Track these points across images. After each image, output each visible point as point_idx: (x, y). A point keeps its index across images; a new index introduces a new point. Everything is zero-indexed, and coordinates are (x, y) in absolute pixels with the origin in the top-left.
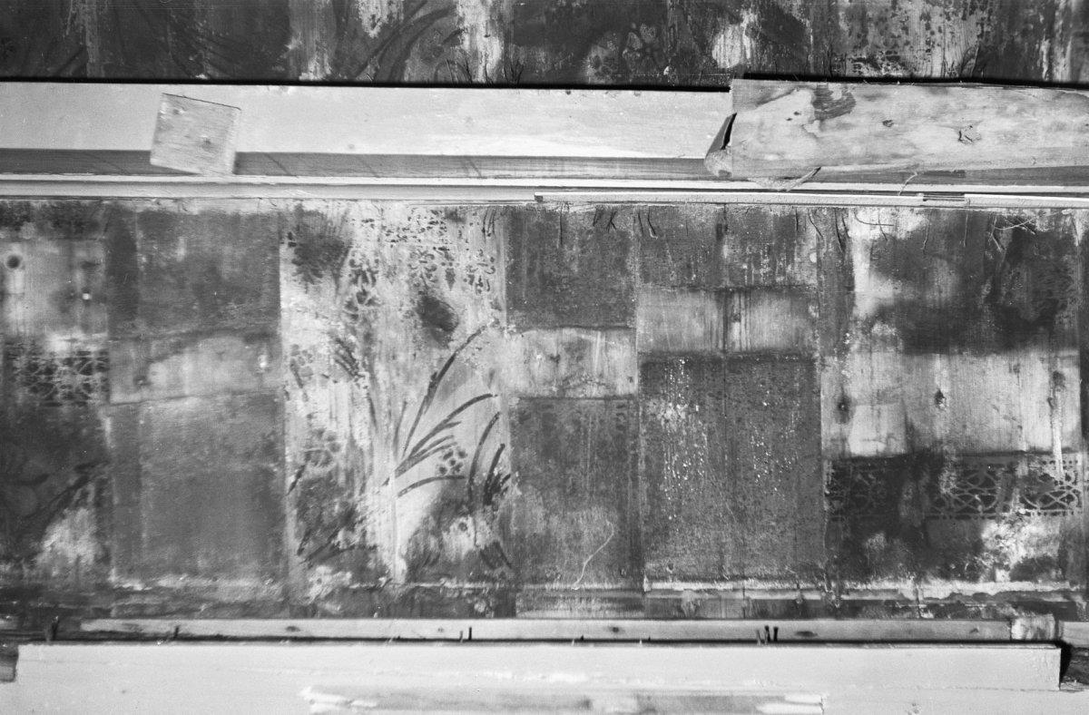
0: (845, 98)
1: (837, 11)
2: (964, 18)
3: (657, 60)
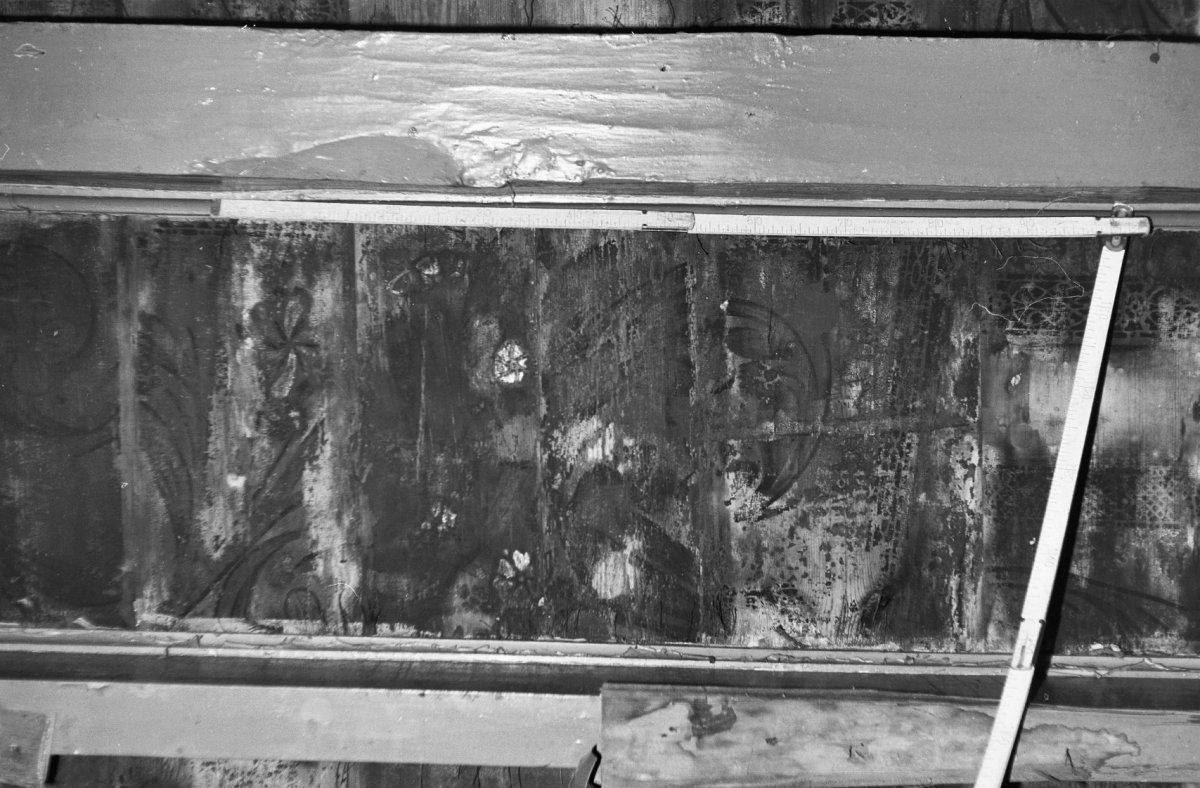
0: (725, 713)
1: (729, 540)
2: (867, 549)
3: (531, 591)
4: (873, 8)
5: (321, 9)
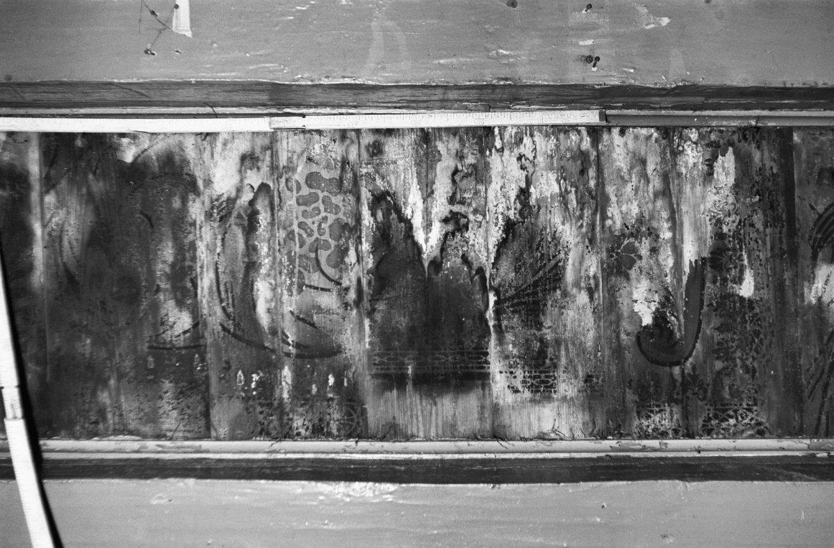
4: (731, 413)
5: (348, 420)
